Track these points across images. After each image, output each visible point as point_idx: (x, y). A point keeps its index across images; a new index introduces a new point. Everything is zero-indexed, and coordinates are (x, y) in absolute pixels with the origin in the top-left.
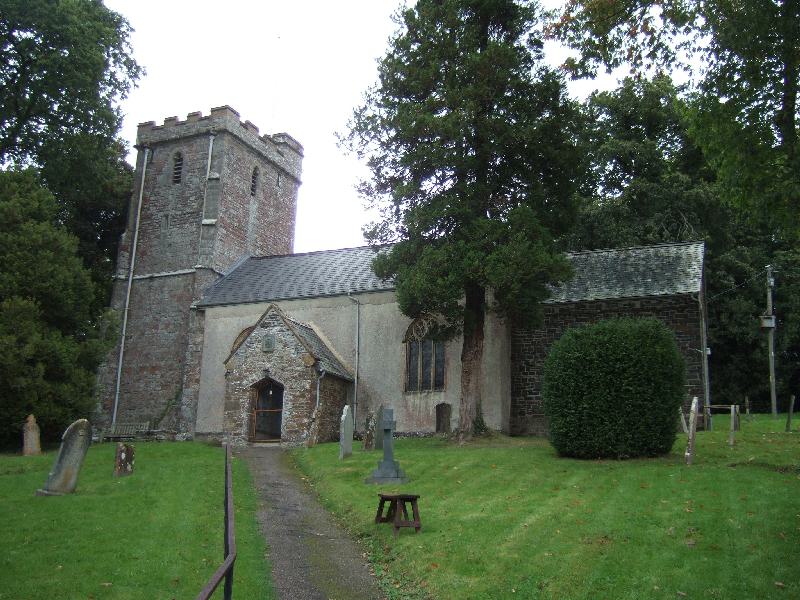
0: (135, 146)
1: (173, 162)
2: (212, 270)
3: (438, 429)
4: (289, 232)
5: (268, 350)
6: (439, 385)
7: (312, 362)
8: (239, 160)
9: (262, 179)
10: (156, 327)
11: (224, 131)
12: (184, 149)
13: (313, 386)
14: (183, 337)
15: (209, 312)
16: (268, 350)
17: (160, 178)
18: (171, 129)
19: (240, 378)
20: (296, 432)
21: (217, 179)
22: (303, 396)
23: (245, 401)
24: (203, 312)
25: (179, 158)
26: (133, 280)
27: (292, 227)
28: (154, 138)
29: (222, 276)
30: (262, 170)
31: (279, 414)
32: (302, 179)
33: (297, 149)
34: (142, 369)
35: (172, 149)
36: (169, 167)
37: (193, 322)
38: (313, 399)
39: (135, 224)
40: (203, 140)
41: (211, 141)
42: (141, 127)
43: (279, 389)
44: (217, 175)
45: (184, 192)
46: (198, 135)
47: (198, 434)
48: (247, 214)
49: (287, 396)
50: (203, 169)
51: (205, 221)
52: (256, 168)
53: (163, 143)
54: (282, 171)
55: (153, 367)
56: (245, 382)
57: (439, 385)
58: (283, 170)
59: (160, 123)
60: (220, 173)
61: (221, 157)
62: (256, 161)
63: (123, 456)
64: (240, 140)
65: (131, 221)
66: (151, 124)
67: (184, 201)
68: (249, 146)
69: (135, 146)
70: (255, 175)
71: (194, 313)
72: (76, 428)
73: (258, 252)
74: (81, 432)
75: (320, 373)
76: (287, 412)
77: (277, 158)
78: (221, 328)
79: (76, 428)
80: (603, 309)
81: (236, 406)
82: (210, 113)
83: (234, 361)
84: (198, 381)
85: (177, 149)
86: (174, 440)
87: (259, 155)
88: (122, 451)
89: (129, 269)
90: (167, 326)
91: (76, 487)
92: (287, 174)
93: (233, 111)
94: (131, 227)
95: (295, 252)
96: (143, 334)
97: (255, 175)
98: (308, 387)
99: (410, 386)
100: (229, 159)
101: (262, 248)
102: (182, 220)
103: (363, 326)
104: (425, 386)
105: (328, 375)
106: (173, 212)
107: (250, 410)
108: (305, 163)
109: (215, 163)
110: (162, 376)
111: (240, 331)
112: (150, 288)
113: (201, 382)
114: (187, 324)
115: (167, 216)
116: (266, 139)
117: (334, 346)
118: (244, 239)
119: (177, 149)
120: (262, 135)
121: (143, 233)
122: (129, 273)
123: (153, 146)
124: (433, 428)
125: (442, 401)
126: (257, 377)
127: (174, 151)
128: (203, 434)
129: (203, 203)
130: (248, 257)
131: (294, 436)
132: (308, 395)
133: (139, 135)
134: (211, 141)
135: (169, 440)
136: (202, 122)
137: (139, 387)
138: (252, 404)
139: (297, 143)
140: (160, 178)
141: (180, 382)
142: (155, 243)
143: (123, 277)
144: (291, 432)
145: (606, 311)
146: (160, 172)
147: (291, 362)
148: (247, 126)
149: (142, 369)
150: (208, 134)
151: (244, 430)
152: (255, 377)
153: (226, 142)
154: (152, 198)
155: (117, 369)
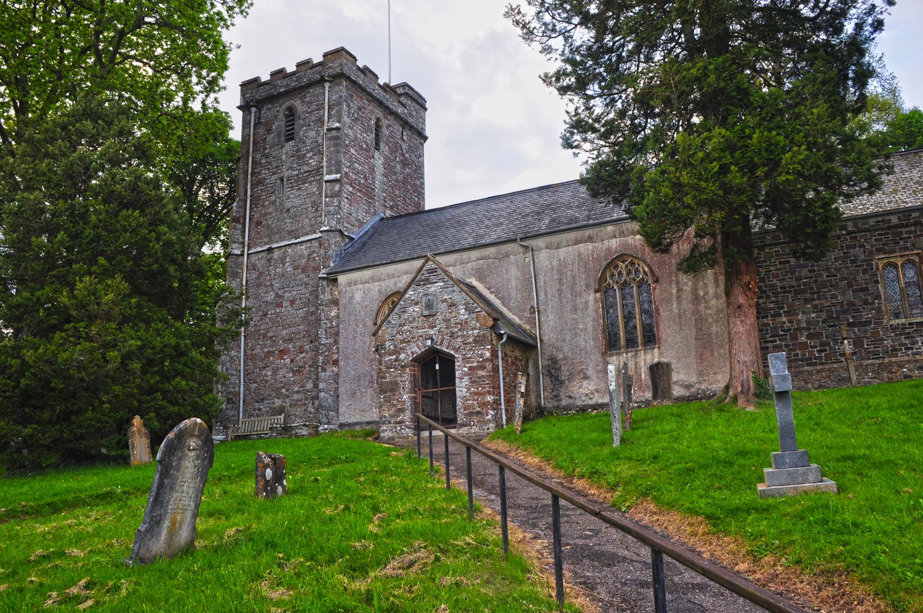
0: (239, 108)
1: (284, 118)
2: (340, 231)
3: (655, 396)
4: (421, 195)
5: (430, 315)
6: (651, 339)
7: (490, 322)
8: (360, 109)
9: (385, 132)
10: (280, 305)
11: (342, 75)
12: (297, 103)
13: (494, 354)
14: (313, 313)
15: (342, 279)
16: (430, 315)
17: (270, 138)
18: (279, 82)
19: (396, 352)
20: (478, 413)
21: (337, 129)
22: (482, 368)
23: (405, 379)
24: (336, 280)
25: (291, 114)
26: (248, 254)
27: (422, 186)
28: (262, 93)
29: (352, 239)
30: (384, 122)
31: (454, 392)
32: (427, 133)
33: (420, 102)
34: (270, 353)
35: (283, 104)
36: (279, 124)
37: (323, 293)
38: (495, 369)
39: (246, 191)
40: (317, 90)
41: (327, 88)
42: (245, 86)
43: (448, 362)
44: (337, 125)
45: (298, 151)
46: (311, 84)
47: (342, 426)
48: (372, 169)
49: (460, 370)
50: (320, 121)
51: (327, 177)
52: (378, 120)
53: (272, 99)
54: (405, 124)
55: (281, 351)
56: (402, 356)
57: (651, 339)
58: (406, 123)
59: (265, 77)
60: (339, 122)
61: (339, 104)
62: (379, 113)
63: (269, 473)
64: (360, 86)
65: (242, 189)
66: (256, 80)
67: (300, 158)
68: (369, 94)
69: (239, 108)
70: (378, 127)
71: (325, 283)
72: (181, 436)
73: (389, 213)
74: (193, 443)
75: (500, 336)
76: (462, 388)
77: (400, 110)
78: (358, 297)
79: (181, 436)
80: (850, 229)
81: (394, 387)
82: (321, 59)
83: (386, 332)
84: (336, 363)
85: (288, 104)
86: (317, 433)
87: (381, 104)
88: (266, 466)
89: (243, 243)
90: (292, 302)
91: (192, 542)
92: (412, 127)
93: (351, 55)
94: (242, 194)
95: (427, 208)
96: (266, 315)
97: (378, 127)
98: (488, 354)
99: (611, 344)
100: (348, 106)
101: (391, 208)
102: (299, 181)
103: (541, 278)
104: (631, 343)
105: (510, 338)
106: (286, 174)
107: (413, 390)
108: (429, 116)
109: (333, 112)
110: (292, 361)
111: (384, 298)
112: (269, 260)
113: (342, 363)
114: (317, 297)
115: (282, 179)
116: (386, 88)
117: (504, 304)
118: (373, 199)
119: (288, 104)
120: (381, 82)
121: (255, 200)
122: (244, 247)
123: (259, 104)
124: (649, 395)
125: (656, 360)
126: (416, 349)
127: (284, 106)
128: (349, 425)
129: (322, 159)
130: (377, 218)
131: (475, 419)
132: (489, 366)
133: (243, 94)
134: (327, 88)
135: (310, 434)
136: (314, 70)
137: (266, 375)
138: (414, 383)
139: (417, 93)
140: (270, 138)
141: (315, 365)
142: (271, 210)
143: (238, 252)
144: (471, 414)
145: (853, 232)
146: (269, 131)
147: (463, 325)
148: (366, 71)
149: (270, 353)
150: (322, 81)
151: (407, 416)
152: (415, 349)
153: (343, 88)
154: (263, 161)
155: (239, 358)
